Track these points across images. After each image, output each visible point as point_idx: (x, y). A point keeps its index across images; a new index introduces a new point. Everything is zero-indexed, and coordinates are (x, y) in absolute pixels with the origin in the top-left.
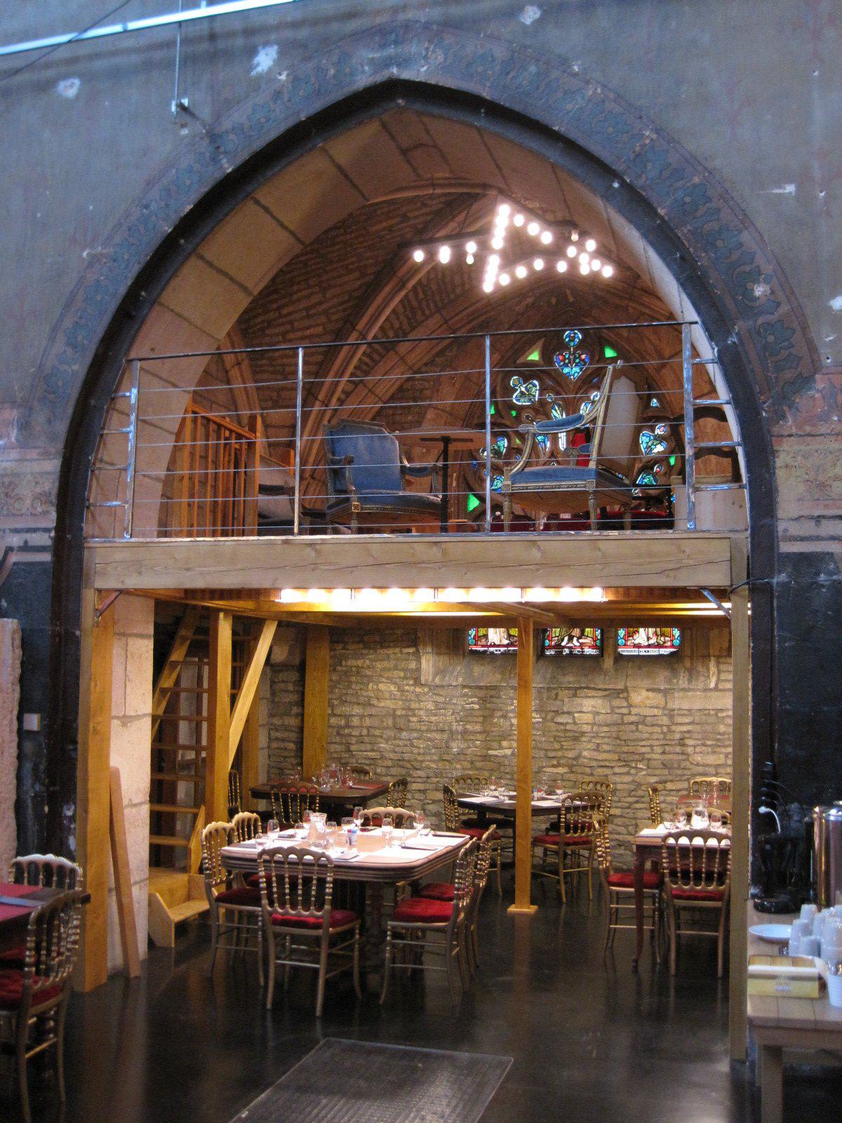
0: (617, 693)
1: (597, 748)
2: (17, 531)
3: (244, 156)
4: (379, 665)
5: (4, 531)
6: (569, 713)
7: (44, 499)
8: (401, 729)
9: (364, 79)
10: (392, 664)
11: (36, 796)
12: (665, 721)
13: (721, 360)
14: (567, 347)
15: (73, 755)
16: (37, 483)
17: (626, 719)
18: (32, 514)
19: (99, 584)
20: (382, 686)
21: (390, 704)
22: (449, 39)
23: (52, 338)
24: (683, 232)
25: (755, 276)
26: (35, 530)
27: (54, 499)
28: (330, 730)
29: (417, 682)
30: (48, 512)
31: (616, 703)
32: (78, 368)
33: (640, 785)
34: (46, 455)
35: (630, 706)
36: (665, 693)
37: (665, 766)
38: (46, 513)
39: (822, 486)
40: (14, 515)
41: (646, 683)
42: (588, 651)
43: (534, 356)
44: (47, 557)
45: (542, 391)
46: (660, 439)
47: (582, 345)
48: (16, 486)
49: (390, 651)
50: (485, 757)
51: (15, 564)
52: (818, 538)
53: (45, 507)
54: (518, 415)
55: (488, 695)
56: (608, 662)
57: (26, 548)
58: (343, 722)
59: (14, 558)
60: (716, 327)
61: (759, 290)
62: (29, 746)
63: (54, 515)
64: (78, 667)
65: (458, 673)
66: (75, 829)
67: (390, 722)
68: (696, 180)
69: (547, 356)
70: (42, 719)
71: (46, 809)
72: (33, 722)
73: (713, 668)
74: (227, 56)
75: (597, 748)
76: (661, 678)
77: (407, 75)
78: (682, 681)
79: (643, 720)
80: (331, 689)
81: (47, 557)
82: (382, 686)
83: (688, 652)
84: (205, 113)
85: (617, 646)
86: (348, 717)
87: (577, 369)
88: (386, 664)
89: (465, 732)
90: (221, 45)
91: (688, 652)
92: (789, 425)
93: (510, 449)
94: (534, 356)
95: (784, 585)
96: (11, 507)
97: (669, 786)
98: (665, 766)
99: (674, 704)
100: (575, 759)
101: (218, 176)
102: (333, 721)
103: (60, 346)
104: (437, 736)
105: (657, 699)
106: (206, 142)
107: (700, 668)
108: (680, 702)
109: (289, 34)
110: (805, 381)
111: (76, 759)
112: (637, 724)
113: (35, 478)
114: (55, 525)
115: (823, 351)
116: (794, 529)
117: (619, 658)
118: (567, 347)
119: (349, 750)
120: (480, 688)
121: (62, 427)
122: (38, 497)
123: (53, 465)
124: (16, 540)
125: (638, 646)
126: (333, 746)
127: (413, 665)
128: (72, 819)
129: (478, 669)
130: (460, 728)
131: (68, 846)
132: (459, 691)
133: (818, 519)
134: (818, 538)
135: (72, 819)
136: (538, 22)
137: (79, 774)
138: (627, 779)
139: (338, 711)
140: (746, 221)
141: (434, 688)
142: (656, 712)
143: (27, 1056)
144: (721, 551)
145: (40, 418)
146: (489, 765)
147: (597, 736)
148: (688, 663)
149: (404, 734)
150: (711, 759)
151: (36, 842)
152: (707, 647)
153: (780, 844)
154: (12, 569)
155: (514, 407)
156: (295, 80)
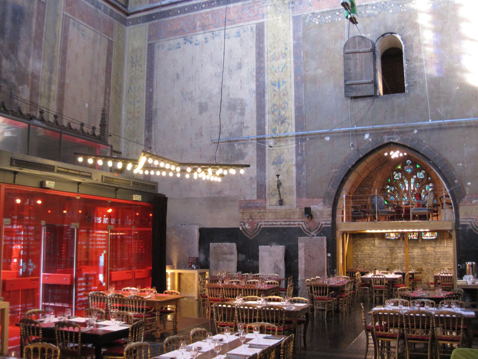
0: (423, 248)
1: (418, 261)
3: (364, 154)
4: (365, 242)
6: (411, 253)
8: (371, 258)
9: (386, 141)
10: (368, 242)
12: (434, 254)
13: (450, 192)
14: (407, 165)
17: (425, 254)
20: (366, 248)
21: (368, 252)
22: (401, 135)
23: (328, 186)
24: (443, 171)
25: (455, 179)
29: (374, 246)
31: (423, 250)
32: (334, 192)
33: (429, 269)
34: (329, 207)
35: (426, 251)
36: (434, 248)
37: (435, 265)
39: (467, 213)
41: (429, 245)
42: (415, 238)
43: (399, 167)
44: (330, 226)
45: (402, 175)
46: (431, 187)
47: (411, 164)
49: (367, 239)
50: (392, 264)
52: (466, 222)
54: (396, 181)
55: (392, 250)
56: (420, 241)
57: (326, 224)
58: (356, 256)
59: (323, 226)
60: (449, 186)
61: (456, 181)
62: (328, 260)
65: (384, 244)
67: (368, 256)
68: (445, 162)
69: (402, 167)
72: (329, 255)
73: (445, 242)
74: (360, 135)
75: (418, 261)
76: (433, 244)
77: (394, 141)
78: (438, 245)
79: (429, 254)
80: (353, 249)
81: (330, 226)
82: (366, 248)
83: (439, 238)
84: (356, 145)
85: (422, 236)
86: (357, 255)
87: (410, 170)
88: (366, 242)
89: (386, 258)
90: (358, 133)
91: (439, 238)
92: (461, 203)
93: (394, 190)
94: (399, 167)
95: (461, 230)
97: (436, 269)
98: (435, 265)
99: (217, 273)
100: (413, 263)
101: (359, 158)
102: (354, 256)
103: (330, 187)
104: (380, 259)
105: (432, 249)
106: (356, 151)
107: (443, 242)
108: (438, 250)
109: (371, 132)
110: (464, 196)
112: (428, 255)
115: (466, 191)
116: (462, 220)
117: (423, 240)
118: (407, 165)
119: (358, 263)
120: (390, 247)
121: (332, 202)
123: (330, 209)
124: (324, 223)
125: (427, 237)
127: (373, 242)
128: (336, 272)
129: (389, 243)
130: (385, 257)
132: (384, 248)
133: (466, 219)
134: (466, 222)
135: (336, 272)
136: (417, 133)
137: (337, 264)
138: (426, 268)
139: (355, 254)
140: (454, 170)
141: (378, 248)
142: (432, 252)
144: (450, 224)
145: (327, 200)
146: (393, 266)
147: (418, 258)
148: (439, 240)
149: (371, 259)
150: (445, 263)
152: (444, 236)
153: (462, 269)
155: (395, 179)
156: (373, 141)
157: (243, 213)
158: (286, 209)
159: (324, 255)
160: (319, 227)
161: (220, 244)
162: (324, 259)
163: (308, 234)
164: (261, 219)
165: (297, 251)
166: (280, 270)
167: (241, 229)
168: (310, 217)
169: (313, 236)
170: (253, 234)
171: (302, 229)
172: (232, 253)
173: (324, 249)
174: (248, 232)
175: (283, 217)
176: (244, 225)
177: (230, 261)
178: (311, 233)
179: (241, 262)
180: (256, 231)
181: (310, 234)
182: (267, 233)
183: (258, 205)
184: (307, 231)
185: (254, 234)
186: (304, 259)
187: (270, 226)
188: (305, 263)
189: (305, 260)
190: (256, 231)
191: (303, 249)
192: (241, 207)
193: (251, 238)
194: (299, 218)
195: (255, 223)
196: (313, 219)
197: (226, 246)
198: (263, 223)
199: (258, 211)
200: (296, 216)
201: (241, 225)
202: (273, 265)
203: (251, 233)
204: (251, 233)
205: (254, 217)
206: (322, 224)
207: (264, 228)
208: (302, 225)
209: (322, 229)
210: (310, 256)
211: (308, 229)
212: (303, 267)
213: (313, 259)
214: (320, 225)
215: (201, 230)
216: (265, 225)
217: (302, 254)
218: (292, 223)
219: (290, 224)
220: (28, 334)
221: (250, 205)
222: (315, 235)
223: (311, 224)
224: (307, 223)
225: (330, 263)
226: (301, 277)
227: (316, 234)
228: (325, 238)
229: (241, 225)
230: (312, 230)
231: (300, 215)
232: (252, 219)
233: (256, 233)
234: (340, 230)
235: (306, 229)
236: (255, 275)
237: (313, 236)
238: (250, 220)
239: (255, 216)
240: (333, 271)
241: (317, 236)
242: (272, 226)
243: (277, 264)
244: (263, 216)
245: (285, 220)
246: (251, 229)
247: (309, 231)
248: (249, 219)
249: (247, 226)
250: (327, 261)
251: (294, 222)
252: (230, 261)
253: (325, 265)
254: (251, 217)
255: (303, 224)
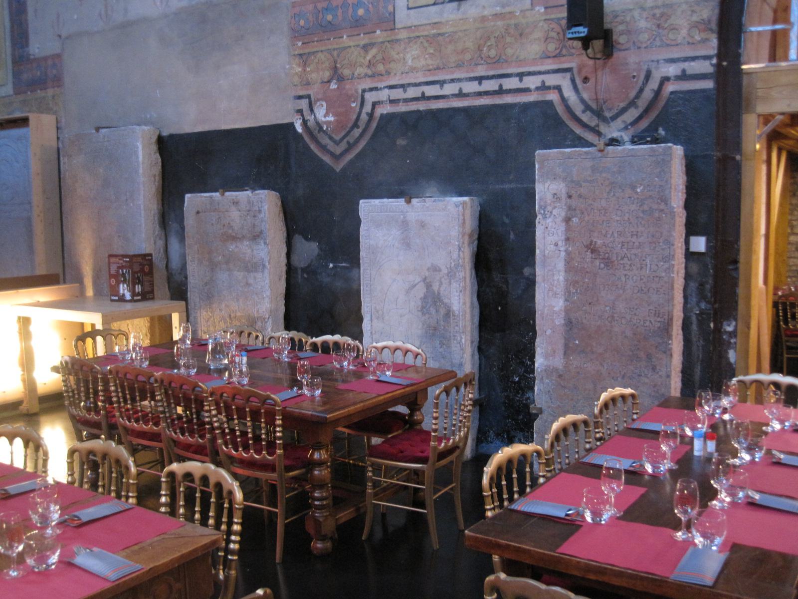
2: (672, 61)
5: (658, 61)
7: (702, 27)
11: (702, 313)
15: (734, 274)
16: (693, 11)
18: (689, 43)
19: (762, 108)
26: (694, 59)
27: (714, 25)
28: (789, 246)
30: (707, 40)
38: (705, 41)
40: (668, 45)
48: (670, 16)
51: (672, 93)
53: (704, 35)
57: (684, 76)
59: (670, 87)
62: (695, 268)
63: (714, 42)
64: (740, 191)
66: (735, 343)
70: (708, 241)
71: (712, 325)
72: (699, 244)
81: (709, 84)
96: (664, 38)
111: (738, 279)
113: (691, 6)
114: (716, 52)
122: (695, 26)
124: (672, 70)
126: (792, 260)
128: (733, 334)
131: (728, 359)
137: (741, 291)
143: (453, 485)
151: (701, 356)
154: (669, 99)
157: (304, 58)
158: (484, 19)
159: (670, 244)
160: (648, 94)
161: (216, 195)
162: (670, 269)
163: (590, 137)
164: (372, 76)
165: (530, 226)
166: (448, 314)
167: (299, 129)
168: (598, 44)
169: (613, 142)
170: (344, 145)
171: (560, 109)
172: (257, 237)
173: (672, 214)
174: (325, 141)
175: (468, 56)
176: (312, 110)
177: (253, 267)
178: (603, 128)
179: (304, 270)
180: (357, 132)
181: (599, 134)
182: (401, 142)
183: (361, 12)
184: (585, 118)
185: (350, 147)
186: (561, 265)
187: (413, 107)
188: (571, 284)
189: (569, 267)
190: (357, 132)
191: (559, 212)
192: (297, 34)
193: (338, 167)
194: (546, 56)
195: (349, 98)
196: (616, 54)
197: (236, 203)
198: (384, 95)
199: (363, 40)
200: (532, 48)
201: (300, 112)
202: (421, 291)
203: (337, 143)
204: (337, 143)
205: (346, 72)
206: (665, 80)
207: (387, 119)
208: (558, 88)
209: (661, 103)
210: (593, 249)
211: (587, 108)
212: (559, 304)
213: (608, 262)
214: (653, 85)
215: (165, 145)
216: (392, 102)
217: (551, 239)
218: (511, 83)
219: (500, 91)
220: (76, 392)
221: (329, 17)
222: (626, 137)
223: (606, 80)
224: (586, 80)
225: (702, 285)
226: (546, 356)
227: (632, 131)
228: (678, 151)
229: (300, 112)
230: (608, 115)
231: (546, 39)
232: (341, 79)
233: (357, 140)
234: (762, 108)
235: (578, 109)
236: (319, 340)
237: (613, 142)
238: (333, 86)
239: (352, 65)
240: (718, 330)
241: (637, 140)
242: (422, 106)
243: (435, 287)
244: (384, 61)
245: (481, 71)
246: (339, 125)
247: (593, 122)
248: (329, 82)
249: (322, 114)
250: (688, 277)
251: (521, 76)
252: (253, 267)
253: (671, 300)
254: (336, 74)
255: (564, 82)
